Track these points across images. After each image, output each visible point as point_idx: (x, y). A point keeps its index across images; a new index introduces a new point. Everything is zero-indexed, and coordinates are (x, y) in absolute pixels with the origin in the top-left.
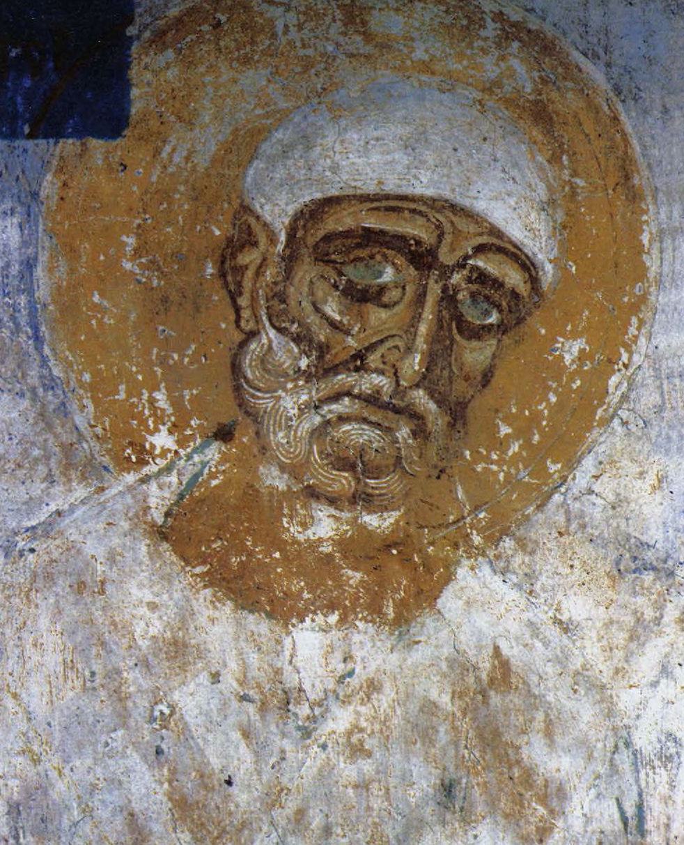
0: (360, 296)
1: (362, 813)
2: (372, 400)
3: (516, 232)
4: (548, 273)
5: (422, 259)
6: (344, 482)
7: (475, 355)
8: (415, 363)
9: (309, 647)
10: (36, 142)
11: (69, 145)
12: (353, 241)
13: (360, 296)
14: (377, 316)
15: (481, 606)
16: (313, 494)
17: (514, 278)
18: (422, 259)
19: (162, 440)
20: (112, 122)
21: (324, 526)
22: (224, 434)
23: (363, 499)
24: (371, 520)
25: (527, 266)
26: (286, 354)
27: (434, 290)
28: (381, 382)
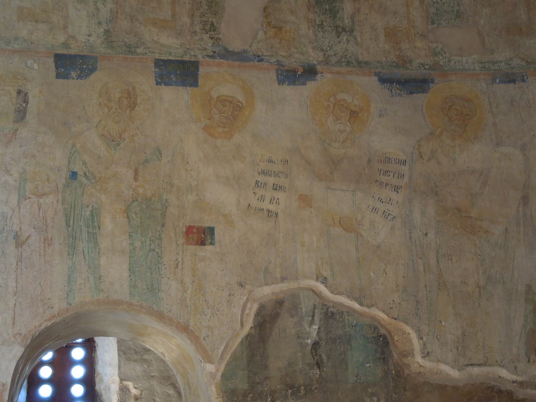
0: (224, 106)
1: (179, 42)
2: (225, 117)
3: (241, 100)
4: (244, 105)
5: (231, 102)
6: (222, 125)
7: (237, 113)
8: (230, 113)
9: (219, 142)
10: (182, 59)
11: (192, 88)
12: (223, 101)
13: (224, 106)
14: (226, 108)
15: (237, 138)
16: (219, 126)
17: (241, 105)
18: (231, 102)
19: (203, 119)
20: (197, 86)
21: (220, 130)
22: (209, 119)
23: (224, 127)
24: (226, 129)
25: (242, 103)
26: (216, 111)
27: (232, 106)
28: (226, 115)
